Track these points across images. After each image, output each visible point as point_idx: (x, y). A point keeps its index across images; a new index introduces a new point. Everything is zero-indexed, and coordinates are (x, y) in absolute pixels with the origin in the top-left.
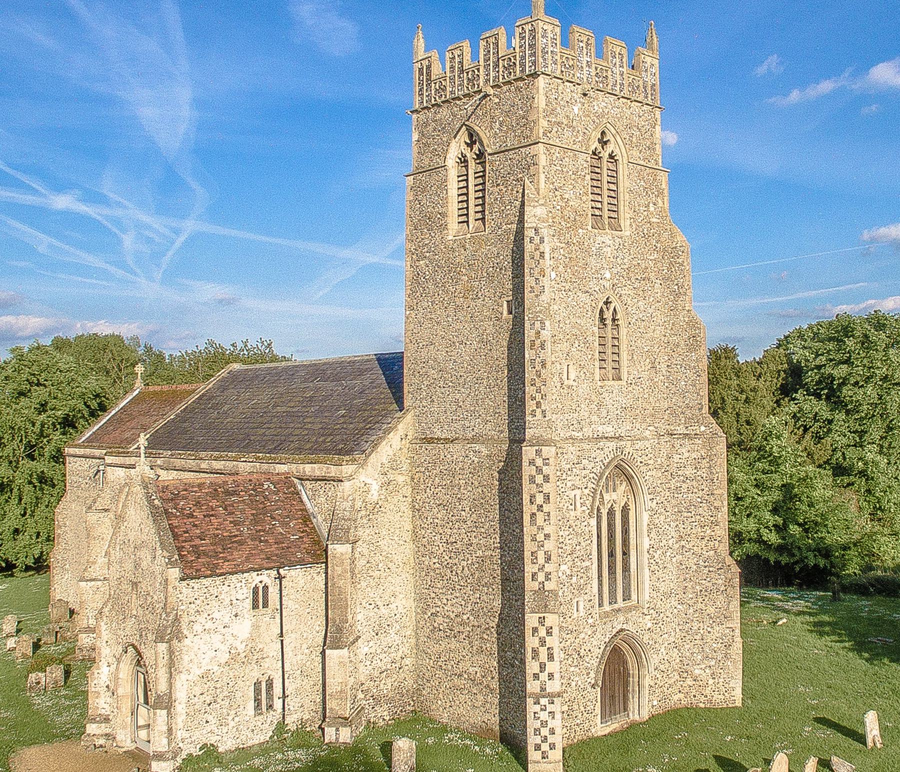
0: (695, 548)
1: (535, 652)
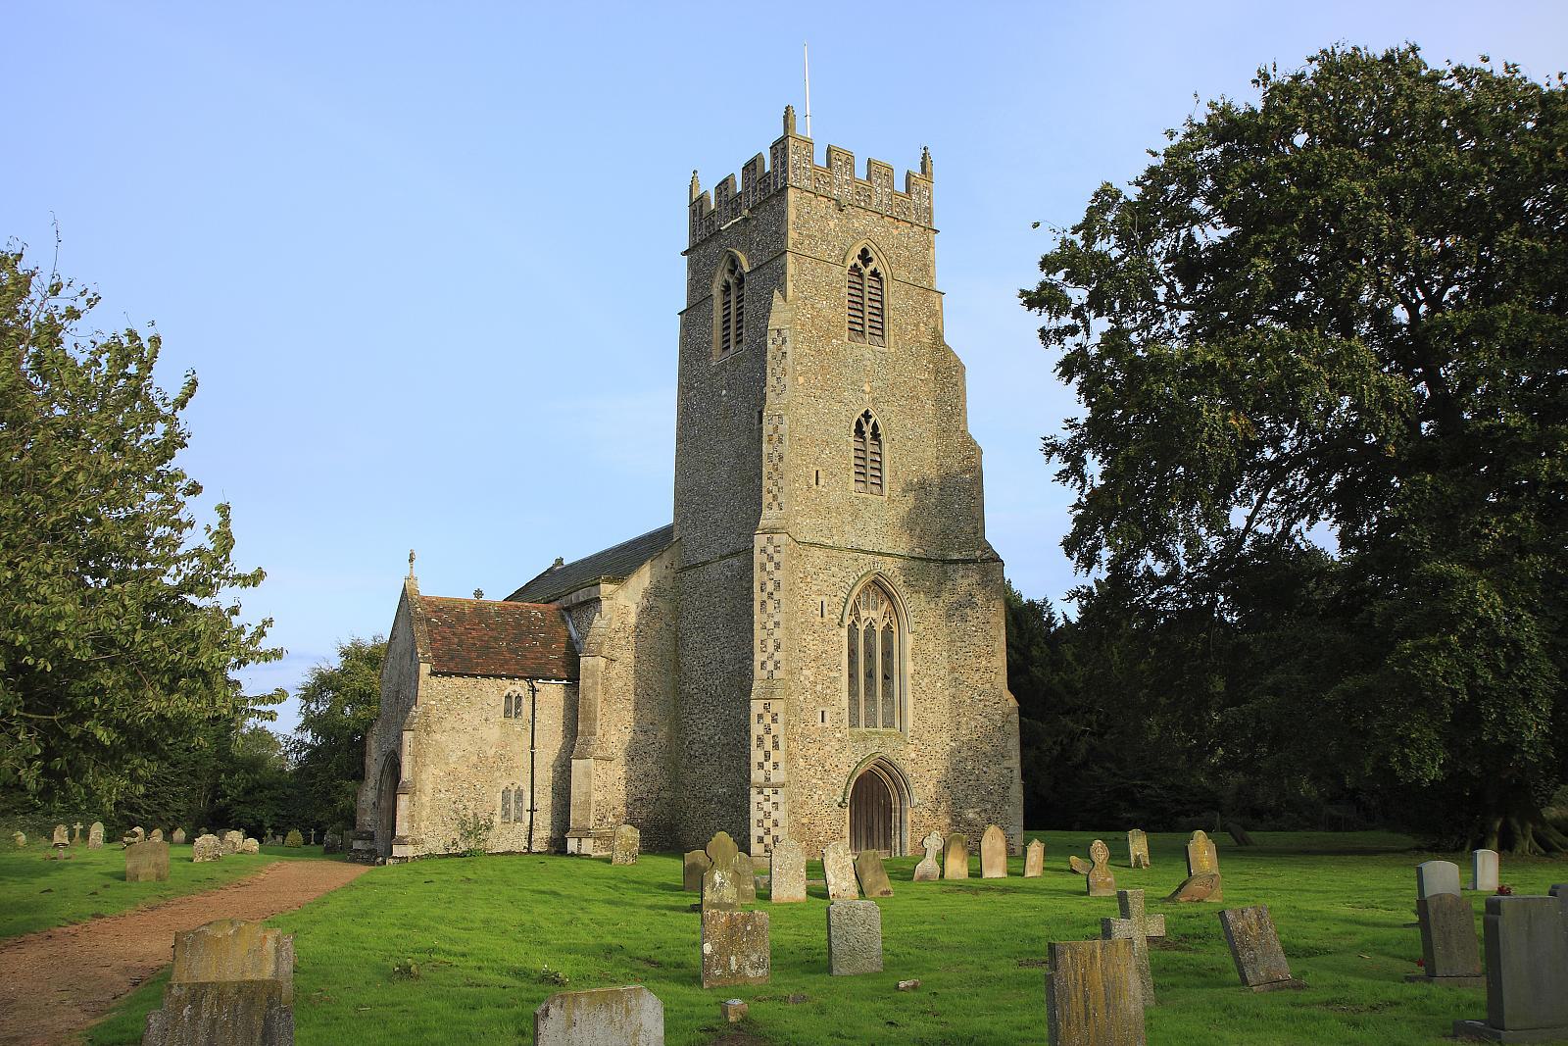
0: (969, 680)
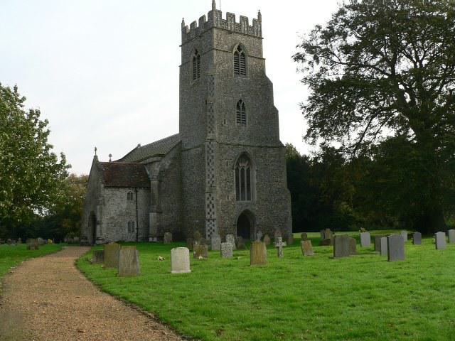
1: (208, 205)
